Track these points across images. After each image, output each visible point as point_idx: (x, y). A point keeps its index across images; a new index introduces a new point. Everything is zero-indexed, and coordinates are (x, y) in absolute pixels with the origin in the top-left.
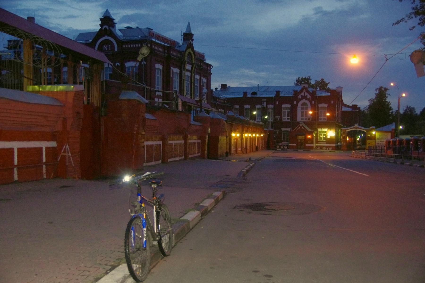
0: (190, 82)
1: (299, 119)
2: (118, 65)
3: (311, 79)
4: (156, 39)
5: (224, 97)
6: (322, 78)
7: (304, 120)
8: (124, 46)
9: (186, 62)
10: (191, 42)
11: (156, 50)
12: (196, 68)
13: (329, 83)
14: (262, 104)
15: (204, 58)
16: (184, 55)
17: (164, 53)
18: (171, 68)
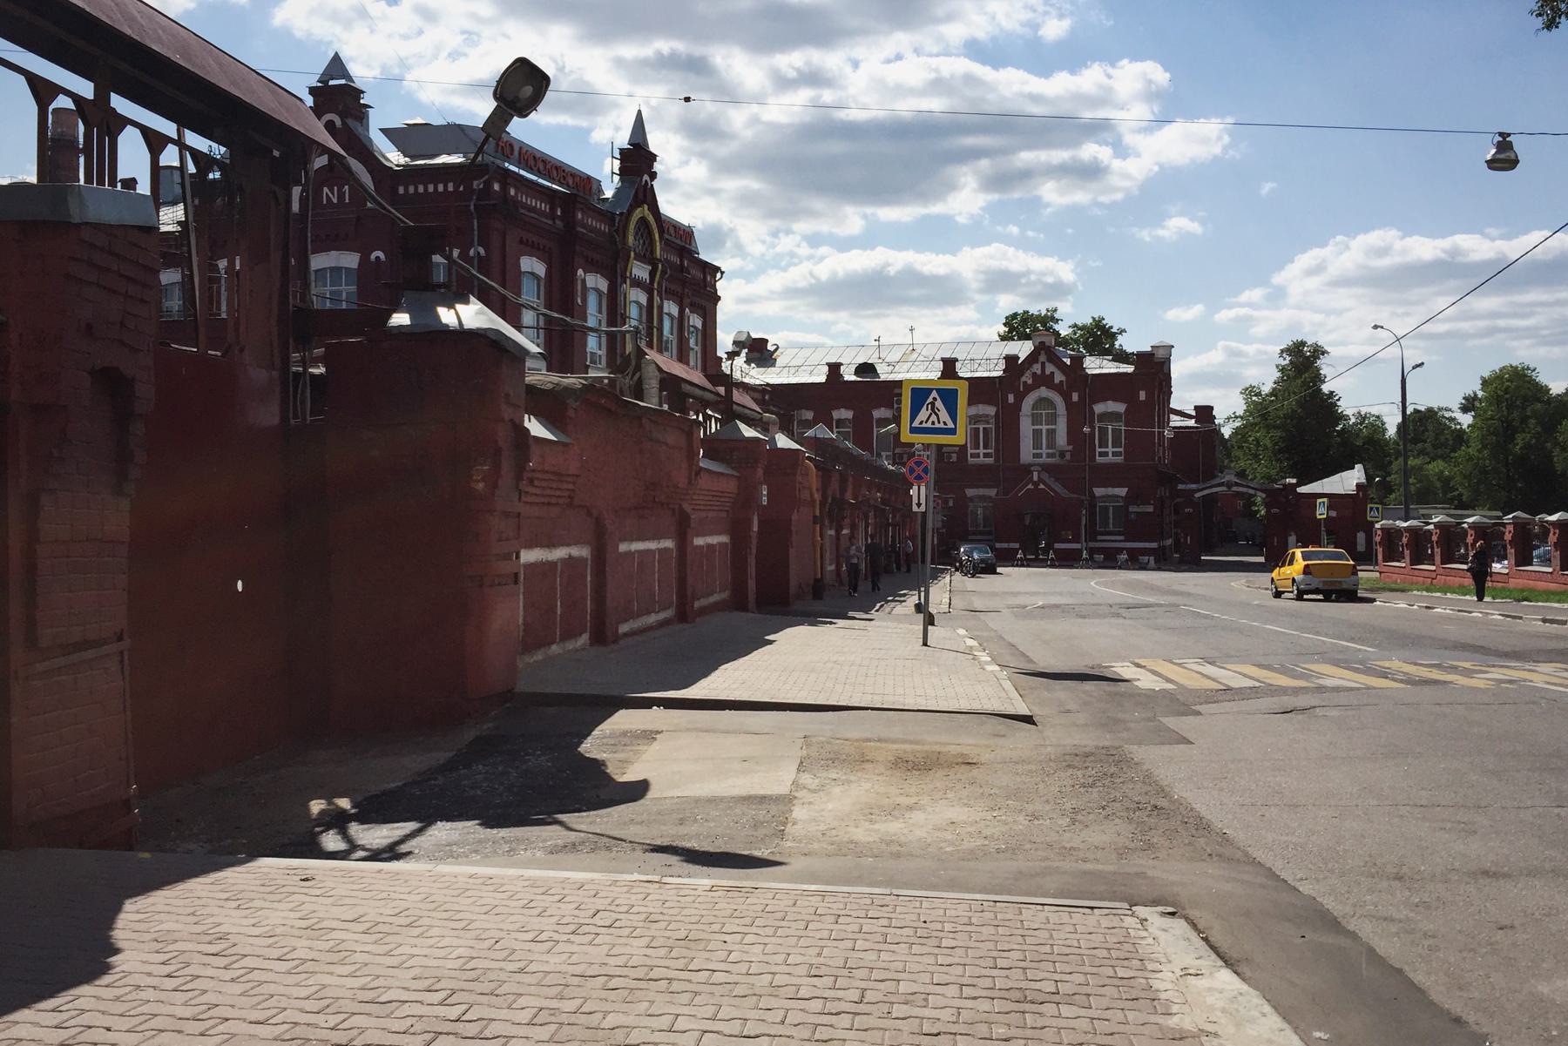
0: (644, 325)
1: (1027, 453)
2: (377, 258)
3: (1058, 320)
4: (519, 168)
5: (762, 383)
6: (1096, 316)
7: (1044, 459)
8: (401, 190)
9: (632, 254)
10: (646, 181)
11: (525, 206)
12: (667, 276)
13: (1122, 331)
14: (895, 406)
15: (693, 241)
16: (626, 227)
17: (553, 219)
18: (578, 274)
